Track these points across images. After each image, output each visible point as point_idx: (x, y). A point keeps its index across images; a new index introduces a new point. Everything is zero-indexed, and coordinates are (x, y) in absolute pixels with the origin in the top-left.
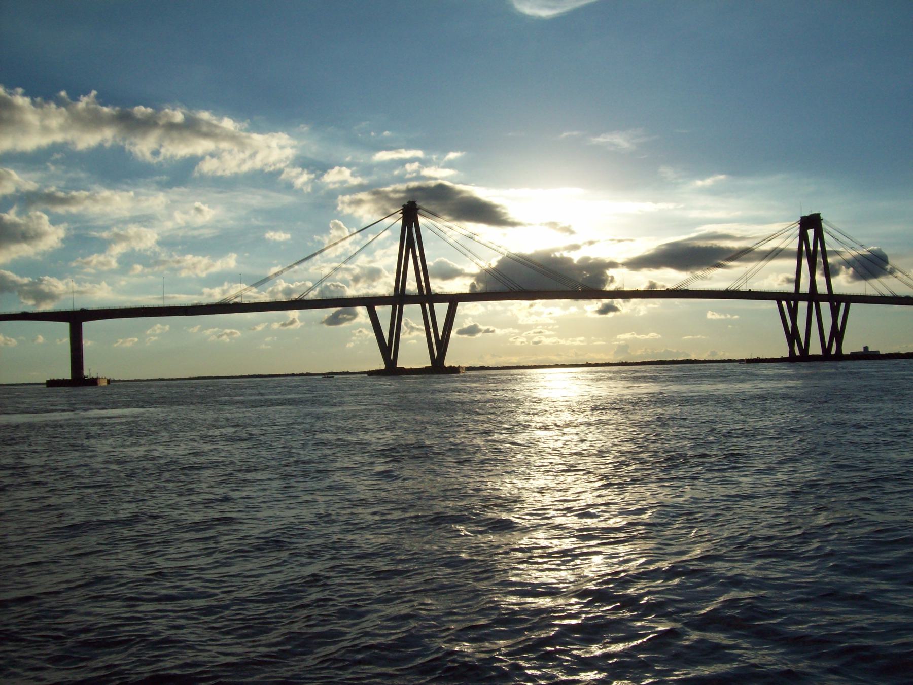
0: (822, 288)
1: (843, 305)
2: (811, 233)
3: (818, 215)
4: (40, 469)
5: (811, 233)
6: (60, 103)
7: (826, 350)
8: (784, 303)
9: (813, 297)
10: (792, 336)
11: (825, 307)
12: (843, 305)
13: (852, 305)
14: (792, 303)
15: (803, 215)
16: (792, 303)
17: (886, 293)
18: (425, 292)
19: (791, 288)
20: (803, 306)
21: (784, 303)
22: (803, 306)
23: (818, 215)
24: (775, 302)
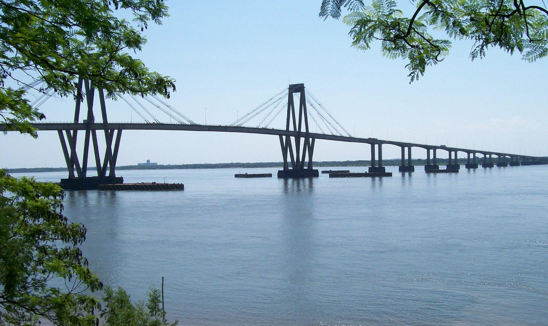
0: (98, 119)
1: (116, 132)
2: (297, 97)
3: (303, 84)
4: (336, 270)
5: (297, 97)
6: (130, 7)
7: (101, 170)
8: (64, 132)
9: (298, 135)
10: (72, 161)
11: (101, 134)
12: (116, 132)
13: (124, 132)
14: (72, 132)
15: (291, 84)
16: (72, 132)
17: (151, 121)
18: (301, 160)
19: (72, 121)
20: (81, 134)
21: (64, 132)
22: (81, 134)
23: (303, 84)
24: (467, 154)
